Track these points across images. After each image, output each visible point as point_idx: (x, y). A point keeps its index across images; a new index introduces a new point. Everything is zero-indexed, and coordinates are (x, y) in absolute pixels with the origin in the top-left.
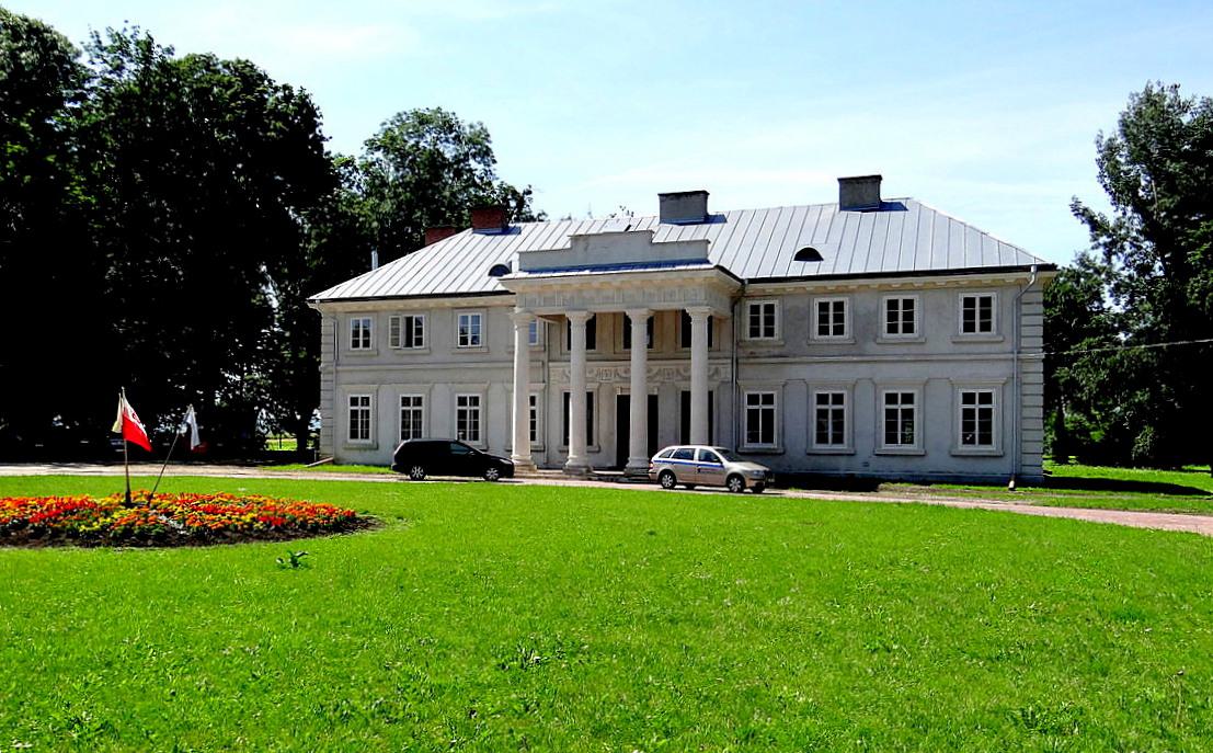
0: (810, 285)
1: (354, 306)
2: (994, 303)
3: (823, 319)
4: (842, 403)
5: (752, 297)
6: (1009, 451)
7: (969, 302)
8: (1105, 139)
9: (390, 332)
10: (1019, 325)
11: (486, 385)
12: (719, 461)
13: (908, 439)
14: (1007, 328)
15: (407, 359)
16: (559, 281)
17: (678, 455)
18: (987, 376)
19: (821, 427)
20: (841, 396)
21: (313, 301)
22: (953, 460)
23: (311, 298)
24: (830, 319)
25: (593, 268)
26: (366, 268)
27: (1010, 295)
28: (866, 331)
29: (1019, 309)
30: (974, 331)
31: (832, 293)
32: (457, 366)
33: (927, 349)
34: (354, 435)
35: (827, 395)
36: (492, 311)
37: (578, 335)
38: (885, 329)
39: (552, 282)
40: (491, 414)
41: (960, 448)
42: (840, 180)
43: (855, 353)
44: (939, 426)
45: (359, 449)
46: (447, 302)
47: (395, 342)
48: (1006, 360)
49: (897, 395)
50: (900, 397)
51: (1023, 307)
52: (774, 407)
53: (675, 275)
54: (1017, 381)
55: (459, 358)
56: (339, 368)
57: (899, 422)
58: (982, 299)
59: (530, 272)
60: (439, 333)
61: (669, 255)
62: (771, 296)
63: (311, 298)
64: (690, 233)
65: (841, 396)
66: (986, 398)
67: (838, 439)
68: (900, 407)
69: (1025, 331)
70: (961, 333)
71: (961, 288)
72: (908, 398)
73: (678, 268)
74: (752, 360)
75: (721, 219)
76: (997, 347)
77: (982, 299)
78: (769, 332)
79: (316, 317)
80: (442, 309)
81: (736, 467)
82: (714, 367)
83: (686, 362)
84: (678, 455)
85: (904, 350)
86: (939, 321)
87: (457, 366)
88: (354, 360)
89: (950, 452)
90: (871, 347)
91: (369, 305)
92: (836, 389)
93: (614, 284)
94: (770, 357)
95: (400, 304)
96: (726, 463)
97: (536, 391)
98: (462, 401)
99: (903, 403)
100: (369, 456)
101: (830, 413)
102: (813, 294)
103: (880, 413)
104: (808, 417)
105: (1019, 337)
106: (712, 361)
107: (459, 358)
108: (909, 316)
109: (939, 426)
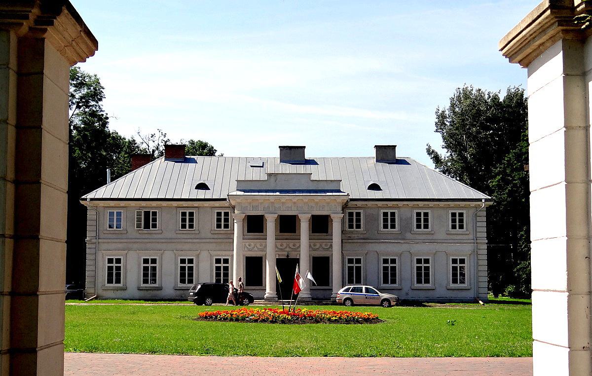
0: (380, 203)
1: (112, 203)
2: (465, 215)
3: (385, 220)
5: (350, 208)
6: (473, 286)
7: (454, 215)
8: (440, 112)
9: (136, 220)
10: (476, 227)
11: (198, 252)
12: (377, 293)
13: (462, 282)
14: (470, 226)
15: (147, 236)
16: (263, 198)
17: (353, 290)
18: (464, 250)
21: (86, 199)
22: (178, 292)
23: (83, 197)
24: (389, 220)
25: (281, 191)
26: (103, 183)
27: (472, 211)
28: (406, 228)
31: (390, 208)
32: (179, 240)
33: (435, 237)
34: (110, 281)
35: (457, 259)
36: (201, 210)
38: (415, 226)
39: (258, 198)
40: (129, 267)
42: (280, 147)
43: (401, 237)
44: (441, 274)
45: (114, 290)
46: (175, 204)
47: (139, 226)
49: (221, 259)
50: (390, 260)
51: (478, 218)
52: (194, 265)
53: (327, 197)
54: (475, 252)
55: (179, 236)
56: (100, 241)
57: (423, 275)
59: (245, 191)
60: (168, 222)
62: (360, 208)
63: (83, 197)
64: (301, 169)
66: (462, 261)
68: (423, 265)
69: (479, 229)
70: (450, 229)
71: (450, 207)
72: (427, 261)
73: (328, 194)
74: (350, 241)
75: (312, 162)
76: (466, 237)
78: (358, 226)
79: (84, 209)
80: (171, 207)
81: (385, 296)
82: (244, 244)
83: (331, 241)
84: (353, 290)
85: (424, 237)
86: (440, 223)
87: (179, 240)
88: (110, 236)
90: (408, 235)
91: (122, 203)
92: (392, 256)
93: (294, 201)
94: (359, 239)
95: (143, 204)
96: (380, 294)
98: (183, 261)
100: (119, 294)
101: (187, 268)
103: (414, 268)
104: (412, 268)
105: (476, 232)
106: (311, 241)
107: (179, 236)
108: (426, 220)
109: (441, 274)
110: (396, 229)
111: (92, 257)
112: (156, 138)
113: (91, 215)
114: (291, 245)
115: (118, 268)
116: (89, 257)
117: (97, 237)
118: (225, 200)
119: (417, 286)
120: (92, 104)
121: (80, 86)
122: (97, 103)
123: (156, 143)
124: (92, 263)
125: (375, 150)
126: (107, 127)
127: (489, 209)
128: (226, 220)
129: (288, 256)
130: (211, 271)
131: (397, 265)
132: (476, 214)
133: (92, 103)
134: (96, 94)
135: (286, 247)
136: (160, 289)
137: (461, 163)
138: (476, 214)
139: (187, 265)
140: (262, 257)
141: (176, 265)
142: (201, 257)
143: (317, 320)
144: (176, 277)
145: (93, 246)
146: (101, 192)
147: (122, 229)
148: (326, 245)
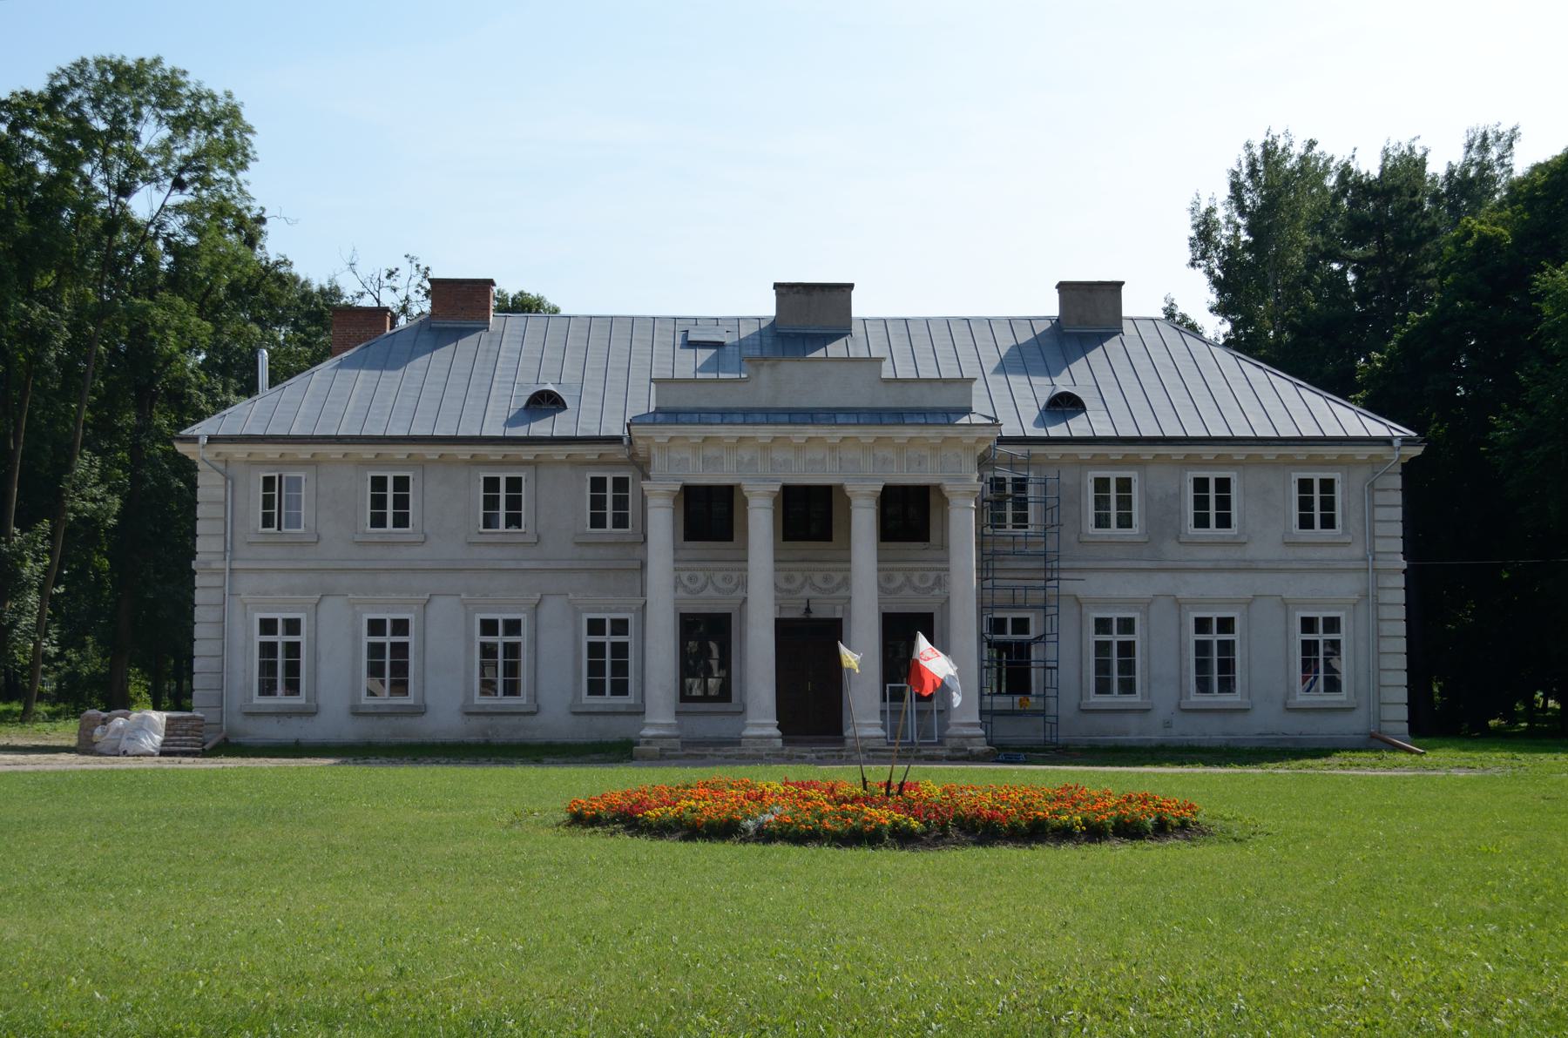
4: (406, 633)
7: (1305, 485)
19: (1102, 667)
20: (625, 622)
22: (475, 722)
23: (183, 433)
29: (1372, 497)
30: (1313, 527)
31: (1114, 464)
34: (267, 688)
37: (864, 521)
41: (1193, 699)
42: (777, 286)
46: (464, 452)
48: (1355, 570)
49: (604, 620)
52: (301, 639)
54: (1370, 599)
58: (1218, 481)
61: (913, 399)
65: (625, 622)
67: (1128, 687)
69: (1380, 529)
70: (1296, 529)
77: (1218, 481)
85: (1216, 553)
89: (1285, 704)
92: (617, 611)
97: (630, 611)
99: (613, 633)
102: (1083, 464)
108: (1224, 503)
110: (1136, 530)
111: (214, 615)
112: (400, 282)
113: (209, 486)
114: (818, 578)
115: (293, 649)
116: (202, 615)
117: (229, 551)
118: (616, 440)
119: (1196, 699)
120: (217, 177)
121: (181, 125)
122: (233, 173)
123: (402, 294)
124: (1386, 628)
125: (1055, 297)
126: (262, 247)
127: (1410, 470)
128: (621, 503)
129: (808, 610)
130: (578, 656)
131: (1137, 637)
132: (1372, 485)
133: (219, 174)
134: (234, 153)
135: (802, 586)
136: (418, 711)
137: (1535, 280)
138: (1372, 485)
139: (1215, 637)
140: (931, 615)
141: (469, 638)
142: (546, 613)
143: (1034, 832)
144: (577, 684)
145: (217, 581)
146: (242, 416)
147: (302, 530)
148: (826, 580)
